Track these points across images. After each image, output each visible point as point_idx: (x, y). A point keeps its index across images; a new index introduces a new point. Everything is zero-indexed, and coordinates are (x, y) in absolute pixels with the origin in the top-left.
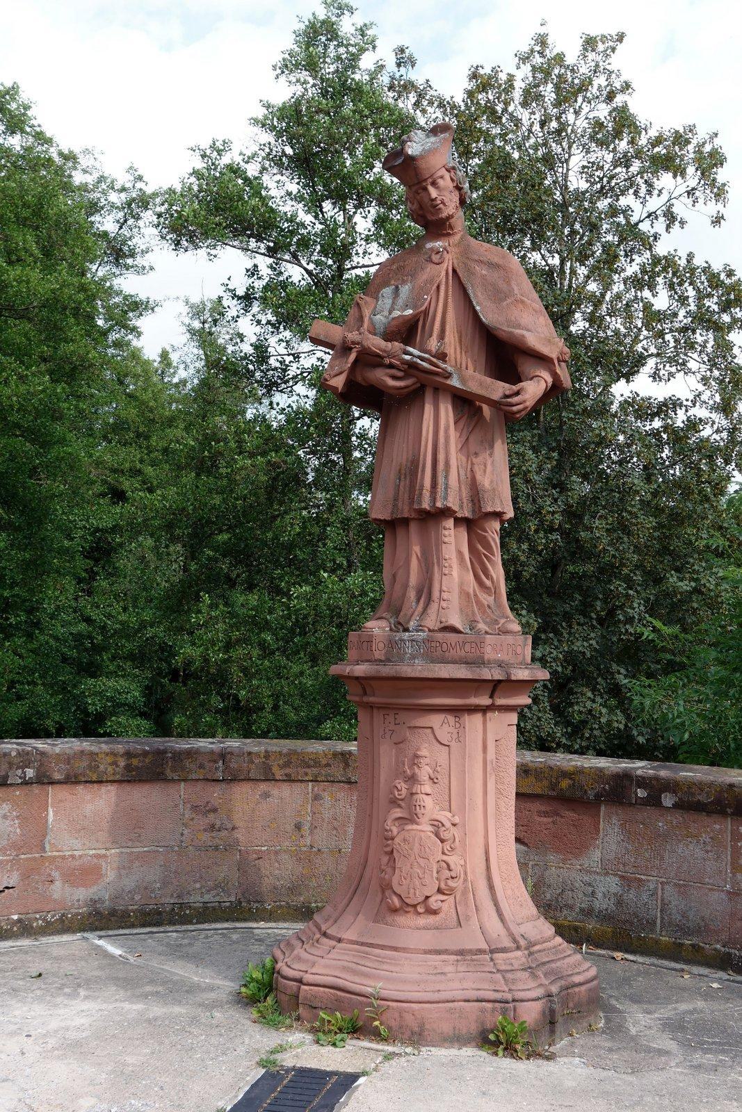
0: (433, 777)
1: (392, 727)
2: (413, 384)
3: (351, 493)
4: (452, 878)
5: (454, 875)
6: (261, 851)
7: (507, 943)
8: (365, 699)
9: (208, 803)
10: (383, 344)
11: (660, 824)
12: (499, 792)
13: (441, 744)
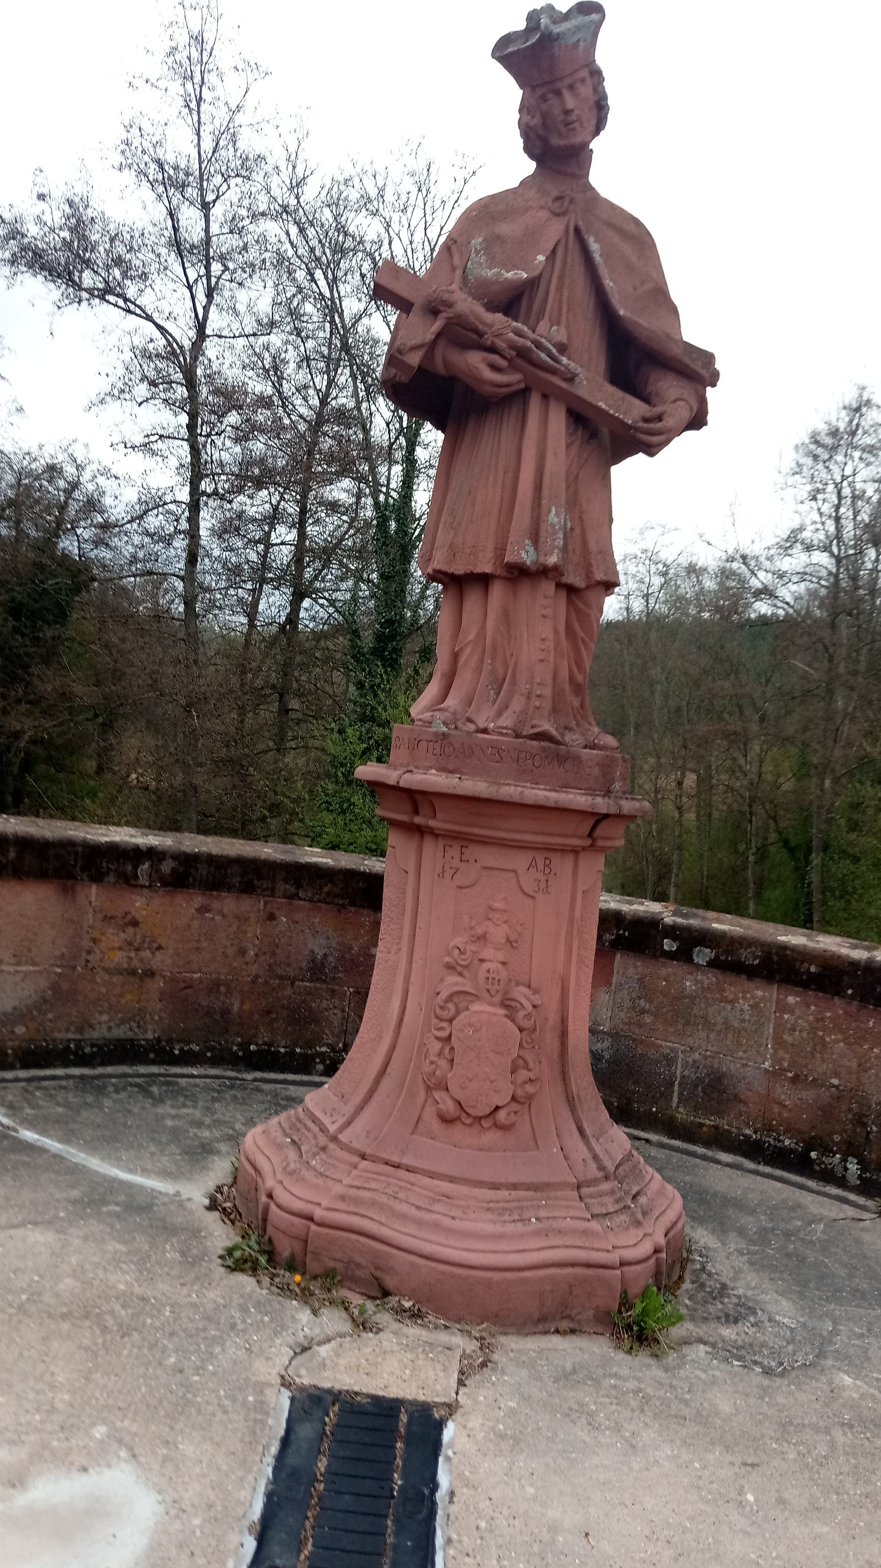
0: (511, 939)
1: (456, 863)
2: (518, 382)
3: (66, 557)
4: (531, 1080)
5: (533, 1078)
6: (192, 979)
7: (593, 1171)
8: (418, 820)
9: (126, 914)
10: (480, 310)
11: (688, 983)
12: (581, 960)
13: (525, 894)
